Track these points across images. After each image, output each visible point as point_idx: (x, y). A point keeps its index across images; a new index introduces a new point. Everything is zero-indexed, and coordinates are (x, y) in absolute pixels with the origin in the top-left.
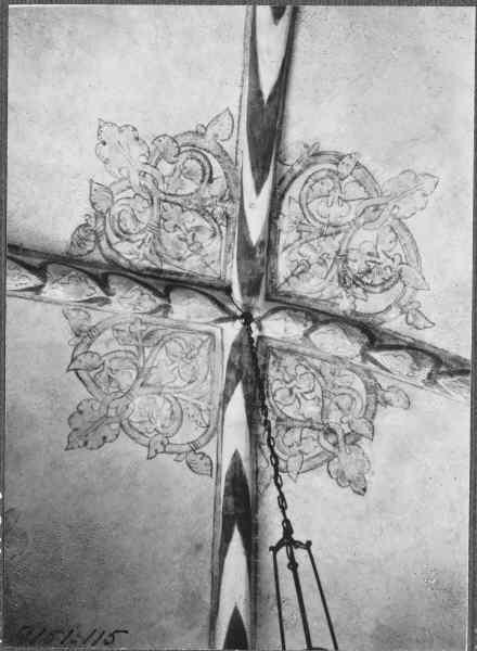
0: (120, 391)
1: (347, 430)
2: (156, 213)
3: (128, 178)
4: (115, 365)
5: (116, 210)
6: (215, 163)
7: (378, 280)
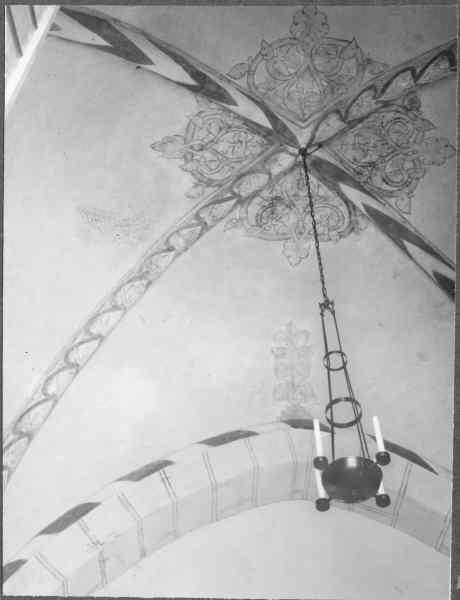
0: (316, 53)
1: (195, 158)
2: (390, 143)
3: (420, 144)
4: (334, 63)
5: (410, 126)
6: (388, 188)
7: (264, 215)
